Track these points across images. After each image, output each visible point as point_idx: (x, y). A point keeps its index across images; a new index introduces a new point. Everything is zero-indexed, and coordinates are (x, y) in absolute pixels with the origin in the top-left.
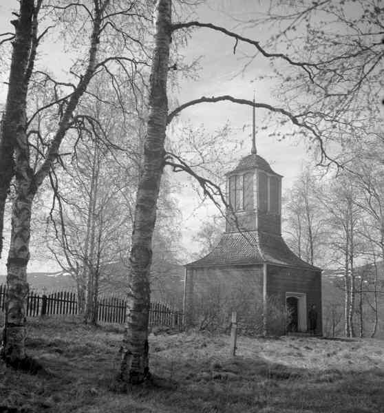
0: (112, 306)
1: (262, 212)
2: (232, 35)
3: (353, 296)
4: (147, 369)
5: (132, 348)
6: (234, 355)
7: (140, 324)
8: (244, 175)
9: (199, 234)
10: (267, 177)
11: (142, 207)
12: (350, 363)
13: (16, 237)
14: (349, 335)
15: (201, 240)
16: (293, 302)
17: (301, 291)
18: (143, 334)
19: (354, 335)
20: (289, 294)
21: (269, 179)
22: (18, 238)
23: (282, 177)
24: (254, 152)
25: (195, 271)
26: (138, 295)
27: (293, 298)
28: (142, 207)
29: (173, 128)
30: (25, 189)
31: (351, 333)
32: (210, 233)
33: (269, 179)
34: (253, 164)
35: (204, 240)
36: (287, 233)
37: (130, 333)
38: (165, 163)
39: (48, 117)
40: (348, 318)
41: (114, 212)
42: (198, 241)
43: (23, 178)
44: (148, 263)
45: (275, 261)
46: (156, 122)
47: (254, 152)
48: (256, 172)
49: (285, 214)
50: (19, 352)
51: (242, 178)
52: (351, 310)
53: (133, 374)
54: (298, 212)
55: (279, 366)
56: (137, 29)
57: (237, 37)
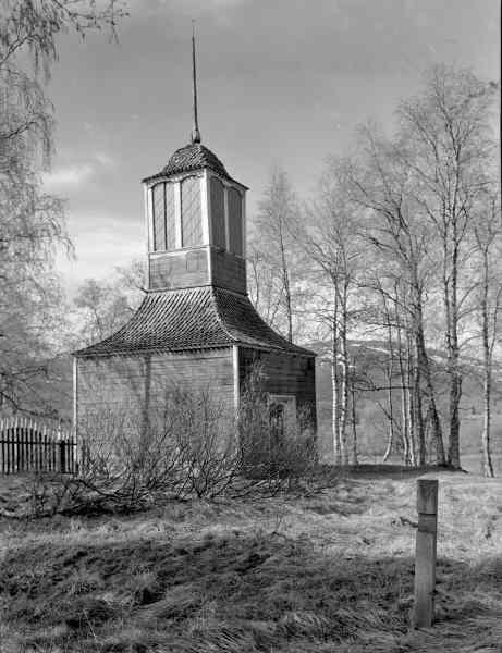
1: (218, 254)
8: (181, 182)
9: (76, 301)
10: (224, 186)
15: (80, 310)
17: (288, 393)
21: (226, 192)
23: (247, 189)
29: (46, 70)
33: (226, 192)
34: (198, 160)
35: (87, 310)
39: (243, 643)
41: (10, 606)
42: (74, 312)
45: (249, 340)
48: (205, 174)
51: (177, 186)
52: (342, 419)
56: (54, 584)
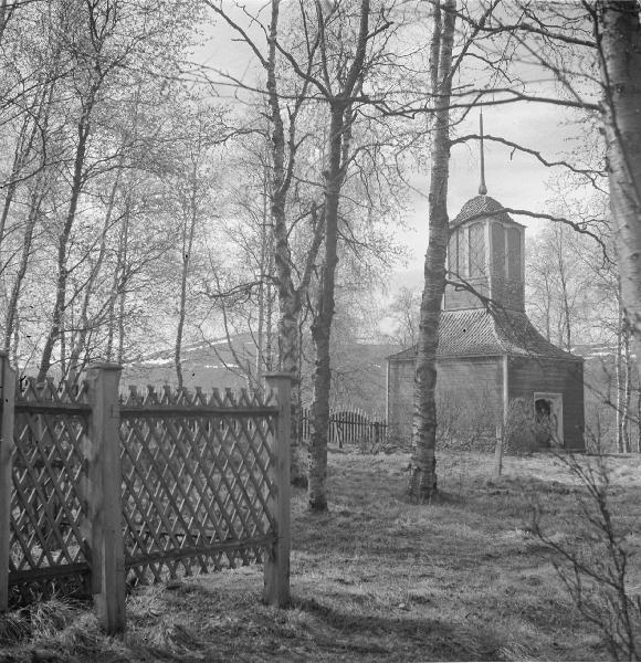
0: (353, 423)
1: (498, 283)
2: (509, 144)
3: (628, 394)
4: (435, 484)
5: (421, 465)
6: (500, 474)
7: (427, 442)
9: (392, 306)
11: (426, 328)
12: (632, 480)
13: (286, 357)
14: (622, 450)
16: (543, 407)
17: (556, 391)
18: (431, 451)
19: (629, 450)
20: (538, 395)
22: (288, 359)
23: (525, 227)
24: (483, 192)
25: (400, 367)
26: (426, 415)
27: (543, 400)
28: (426, 328)
30: (291, 306)
31: (624, 446)
32: (408, 305)
35: (400, 314)
36: (533, 309)
37: (419, 450)
38: (446, 283)
40: (621, 426)
43: (288, 295)
44: (433, 384)
46: (438, 243)
47: (483, 192)
49: (530, 275)
50: (297, 471)
51: (466, 231)
53: (424, 488)
54: (545, 272)
55: (555, 483)
57: (516, 146)
